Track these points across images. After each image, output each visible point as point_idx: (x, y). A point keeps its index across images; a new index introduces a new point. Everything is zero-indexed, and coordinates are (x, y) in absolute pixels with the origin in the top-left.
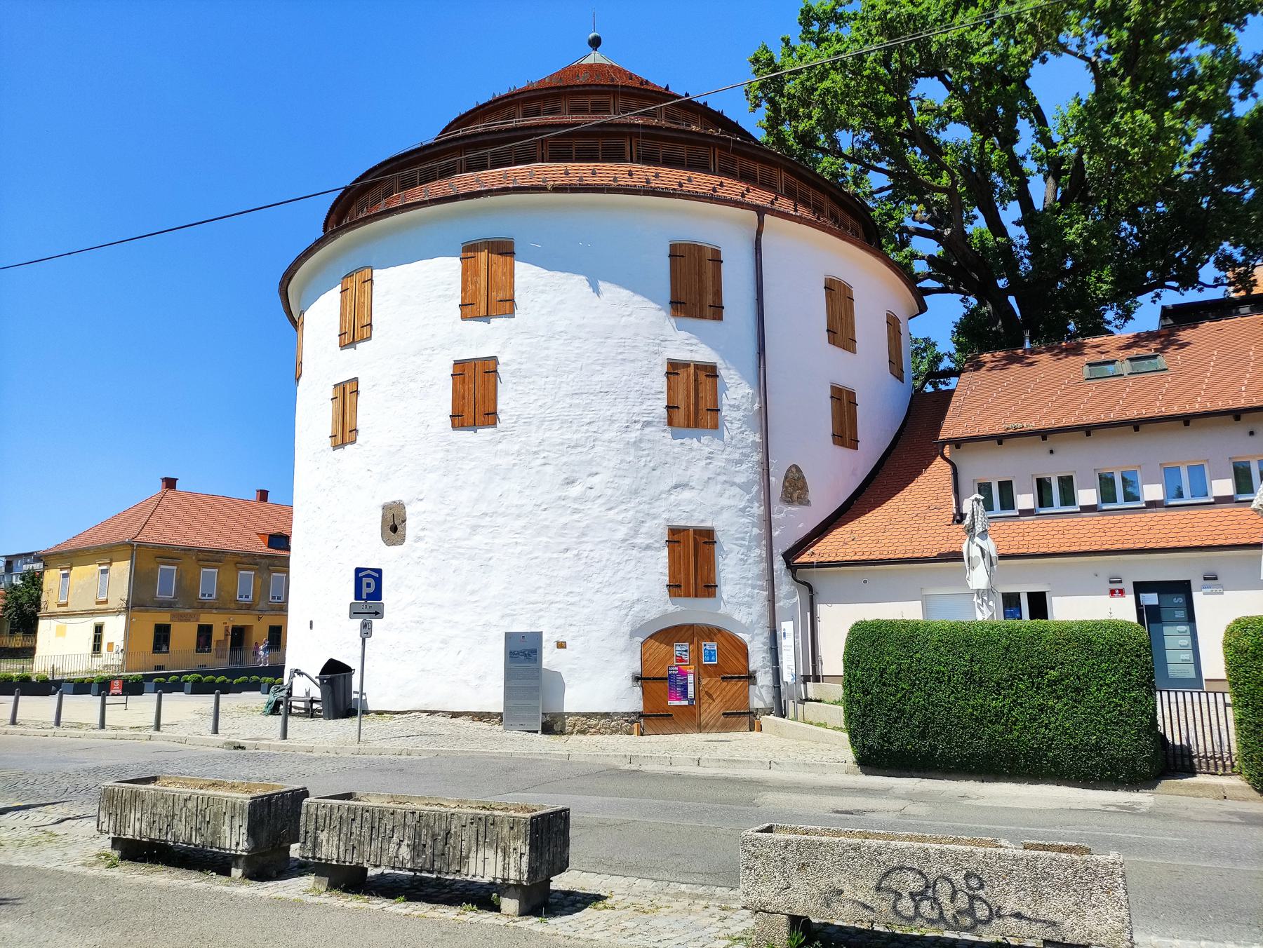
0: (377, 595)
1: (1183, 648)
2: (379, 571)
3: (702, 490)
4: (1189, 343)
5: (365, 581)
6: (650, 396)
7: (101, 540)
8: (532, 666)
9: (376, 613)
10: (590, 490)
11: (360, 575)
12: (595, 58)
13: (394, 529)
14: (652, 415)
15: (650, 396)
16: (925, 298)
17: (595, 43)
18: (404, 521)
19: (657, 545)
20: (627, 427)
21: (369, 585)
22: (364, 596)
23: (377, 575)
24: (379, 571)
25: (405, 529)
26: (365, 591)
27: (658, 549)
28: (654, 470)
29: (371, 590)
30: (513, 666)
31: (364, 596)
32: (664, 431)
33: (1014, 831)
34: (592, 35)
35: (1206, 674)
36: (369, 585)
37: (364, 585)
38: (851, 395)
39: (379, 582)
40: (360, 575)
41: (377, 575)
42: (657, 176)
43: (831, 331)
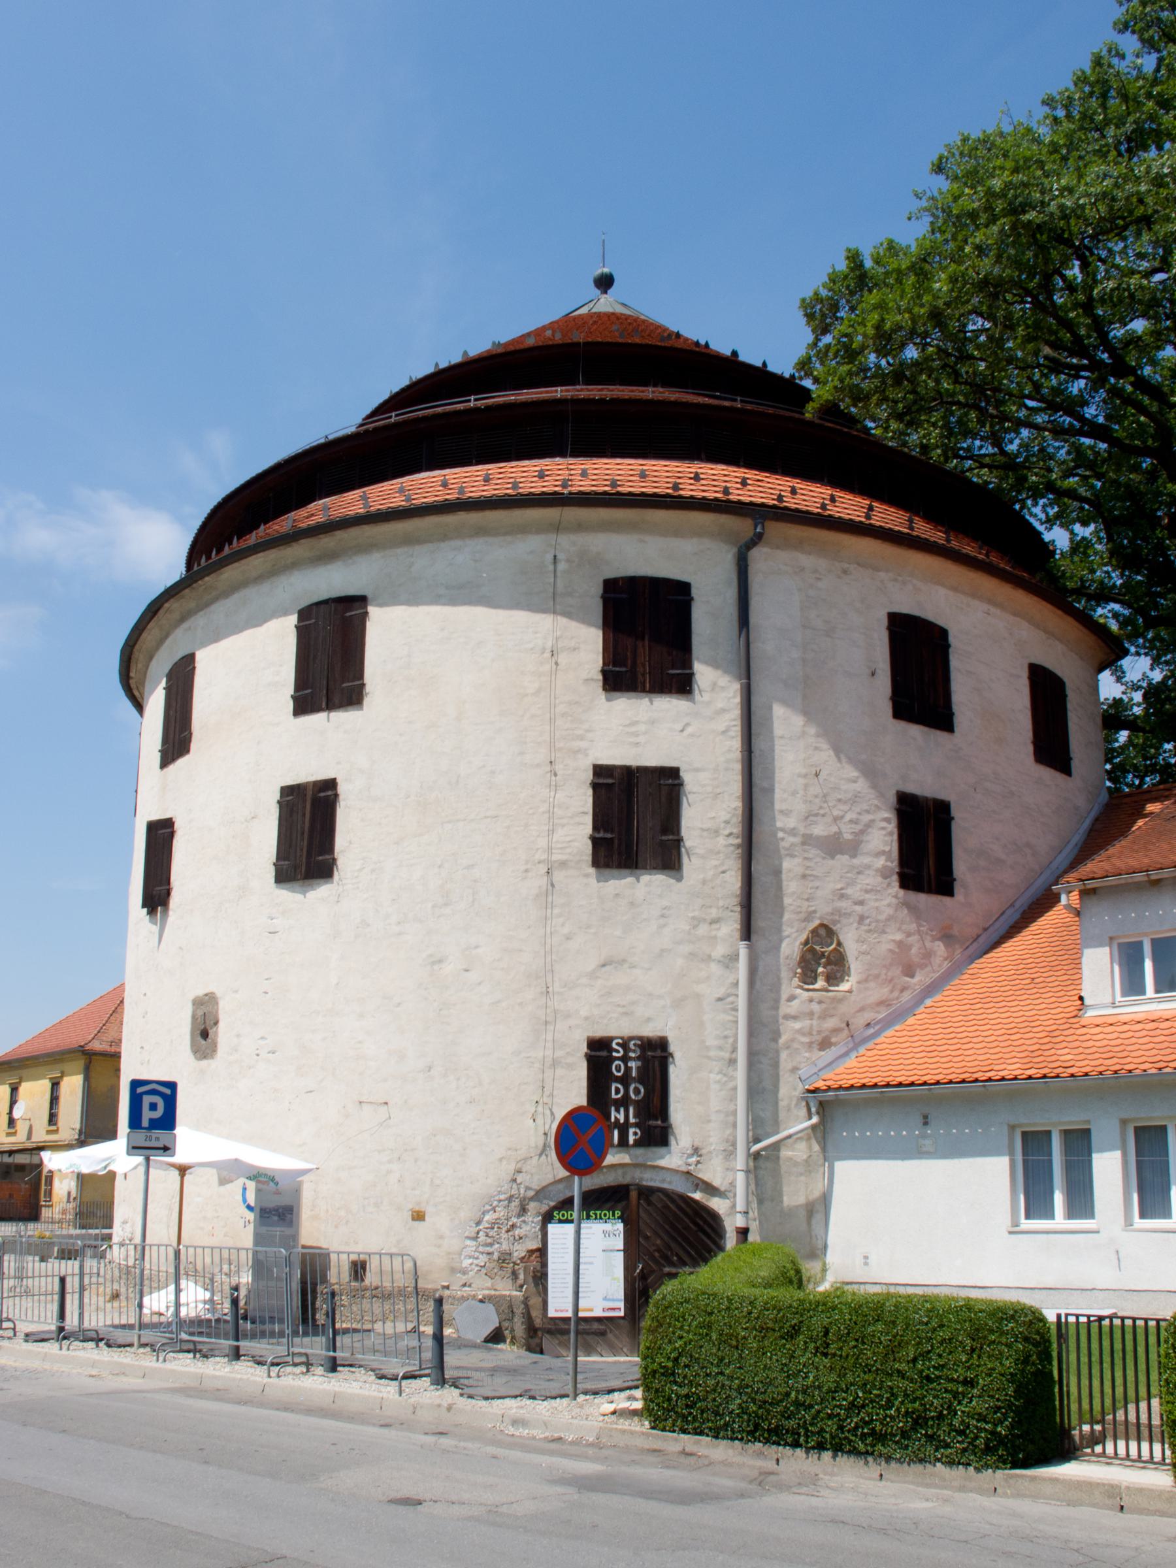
1: (463, 1344)
2: (172, 1086)
3: (650, 969)
4: (328, 721)
5: (147, 1100)
6: (564, 821)
7: (52, 1045)
8: (288, 1231)
9: (166, 1149)
11: (140, 1090)
12: (606, 304)
13: (205, 1034)
14: (568, 850)
15: (564, 821)
17: (605, 283)
18: (216, 1023)
19: (570, 1060)
20: (526, 871)
21: (153, 1107)
22: (145, 1123)
23: (168, 1091)
24: (172, 1086)
25: (216, 1033)
26: (147, 1115)
27: (570, 1066)
28: (568, 939)
30: (264, 1230)
31: (145, 1123)
32: (587, 876)
34: (599, 271)
35: (1107, 1452)
40: (140, 1090)
41: (168, 1091)
42: (584, 474)
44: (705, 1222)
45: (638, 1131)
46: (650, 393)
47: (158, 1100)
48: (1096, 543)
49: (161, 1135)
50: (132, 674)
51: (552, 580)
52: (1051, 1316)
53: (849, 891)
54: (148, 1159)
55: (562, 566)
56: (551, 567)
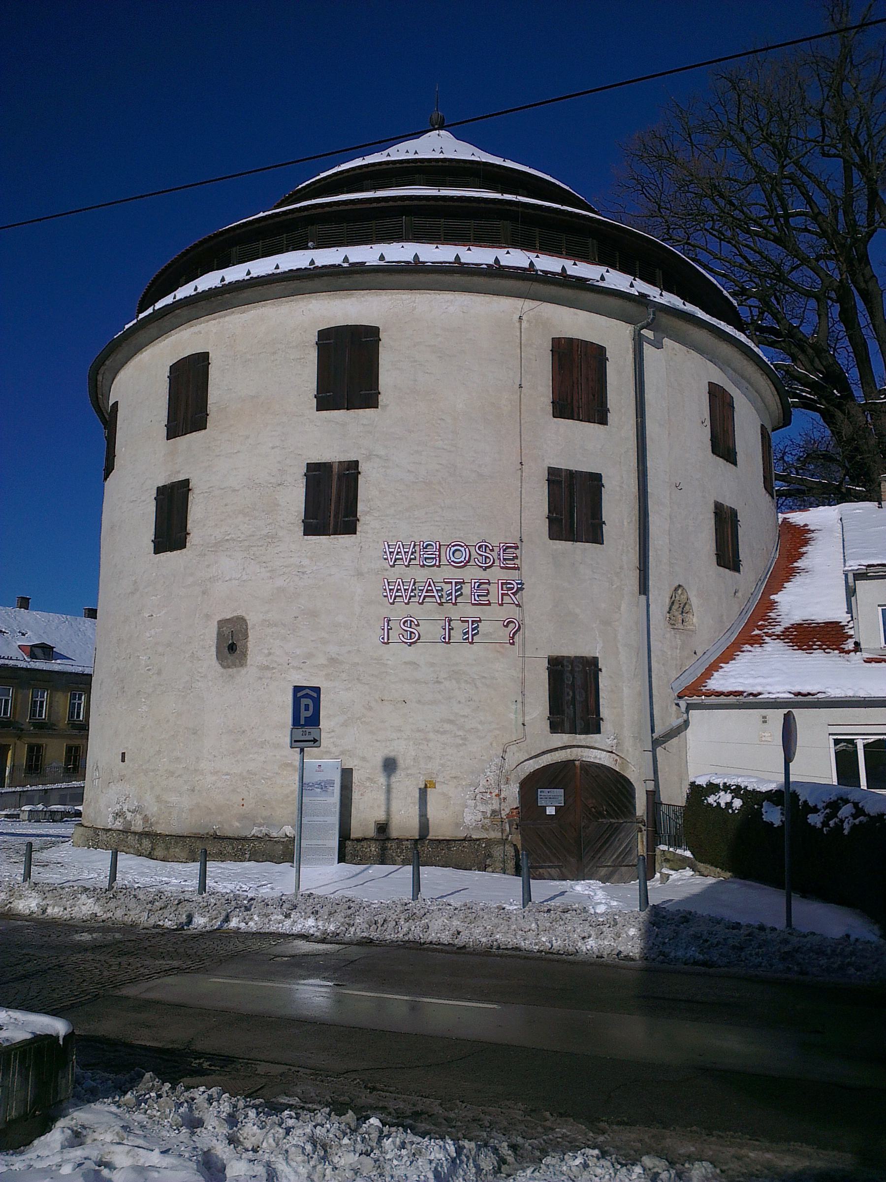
0: (314, 721)
2: (317, 690)
5: (304, 701)
9: (315, 741)
10: (295, 615)
11: (299, 695)
13: (232, 648)
16: (532, 881)
21: (307, 708)
22: (302, 722)
23: (315, 695)
24: (317, 690)
26: (304, 714)
29: (309, 714)
31: (302, 722)
33: (680, 847)
36: (307, 708)
37: (303, 707)
38: (734, 513)
39: (317, 702)
40: (299, 695)
41: (315, 695)
43: (718, 556)
44: (623, 786)
45: (582, 722)
46: (509, 164)
47: (309, 701)
48: (829, 827)
49: (313, 731)
50: (107, 362)
51: (518, 334)
52: (802, 799)
53: (281, 917)
54: (302, 750)
55: (525, 324)
56: (518, 324)
